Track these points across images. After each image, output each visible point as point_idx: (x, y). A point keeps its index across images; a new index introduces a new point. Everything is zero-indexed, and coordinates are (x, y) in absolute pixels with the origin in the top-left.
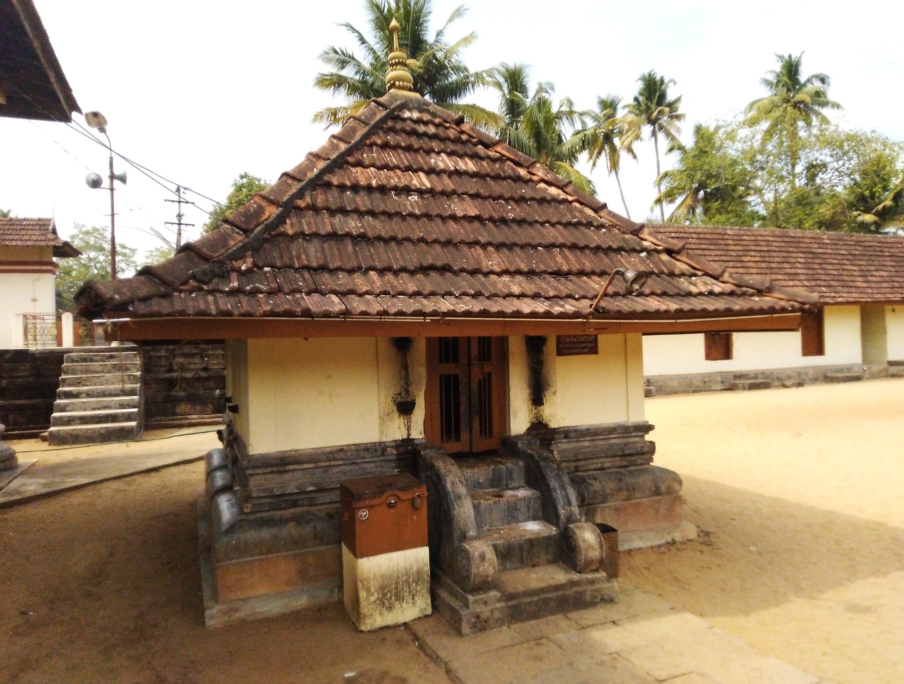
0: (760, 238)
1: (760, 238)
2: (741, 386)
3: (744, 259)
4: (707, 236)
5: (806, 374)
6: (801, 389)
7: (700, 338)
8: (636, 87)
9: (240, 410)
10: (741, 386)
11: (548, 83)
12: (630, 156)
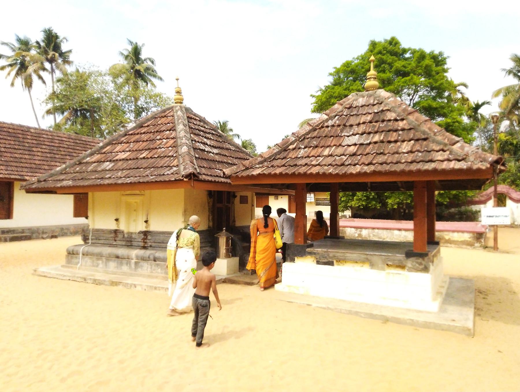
0: (56, 138)
1: (56, 138)
2: (3, 238)
3: (34, 149)
4: (10, 130)
5: (68, 229)
6: (54, 240)
7: (72, 197)
8: (40, 37)
9: (206, 193)
10: (3, 238)
11: (302, 125)
12: (40, 82)
